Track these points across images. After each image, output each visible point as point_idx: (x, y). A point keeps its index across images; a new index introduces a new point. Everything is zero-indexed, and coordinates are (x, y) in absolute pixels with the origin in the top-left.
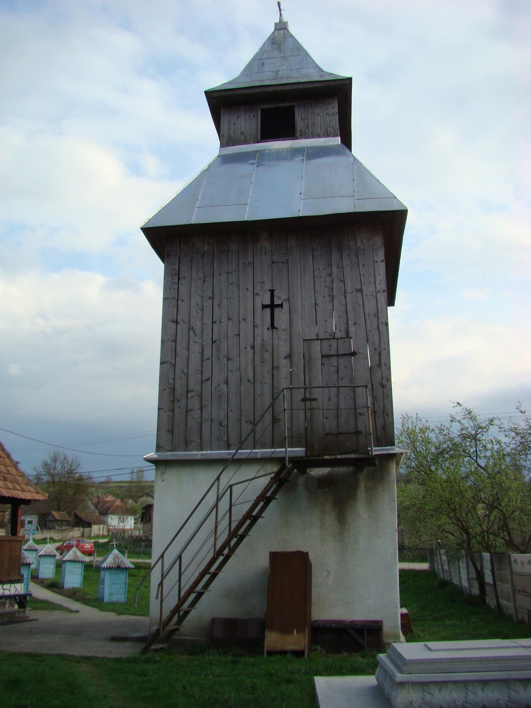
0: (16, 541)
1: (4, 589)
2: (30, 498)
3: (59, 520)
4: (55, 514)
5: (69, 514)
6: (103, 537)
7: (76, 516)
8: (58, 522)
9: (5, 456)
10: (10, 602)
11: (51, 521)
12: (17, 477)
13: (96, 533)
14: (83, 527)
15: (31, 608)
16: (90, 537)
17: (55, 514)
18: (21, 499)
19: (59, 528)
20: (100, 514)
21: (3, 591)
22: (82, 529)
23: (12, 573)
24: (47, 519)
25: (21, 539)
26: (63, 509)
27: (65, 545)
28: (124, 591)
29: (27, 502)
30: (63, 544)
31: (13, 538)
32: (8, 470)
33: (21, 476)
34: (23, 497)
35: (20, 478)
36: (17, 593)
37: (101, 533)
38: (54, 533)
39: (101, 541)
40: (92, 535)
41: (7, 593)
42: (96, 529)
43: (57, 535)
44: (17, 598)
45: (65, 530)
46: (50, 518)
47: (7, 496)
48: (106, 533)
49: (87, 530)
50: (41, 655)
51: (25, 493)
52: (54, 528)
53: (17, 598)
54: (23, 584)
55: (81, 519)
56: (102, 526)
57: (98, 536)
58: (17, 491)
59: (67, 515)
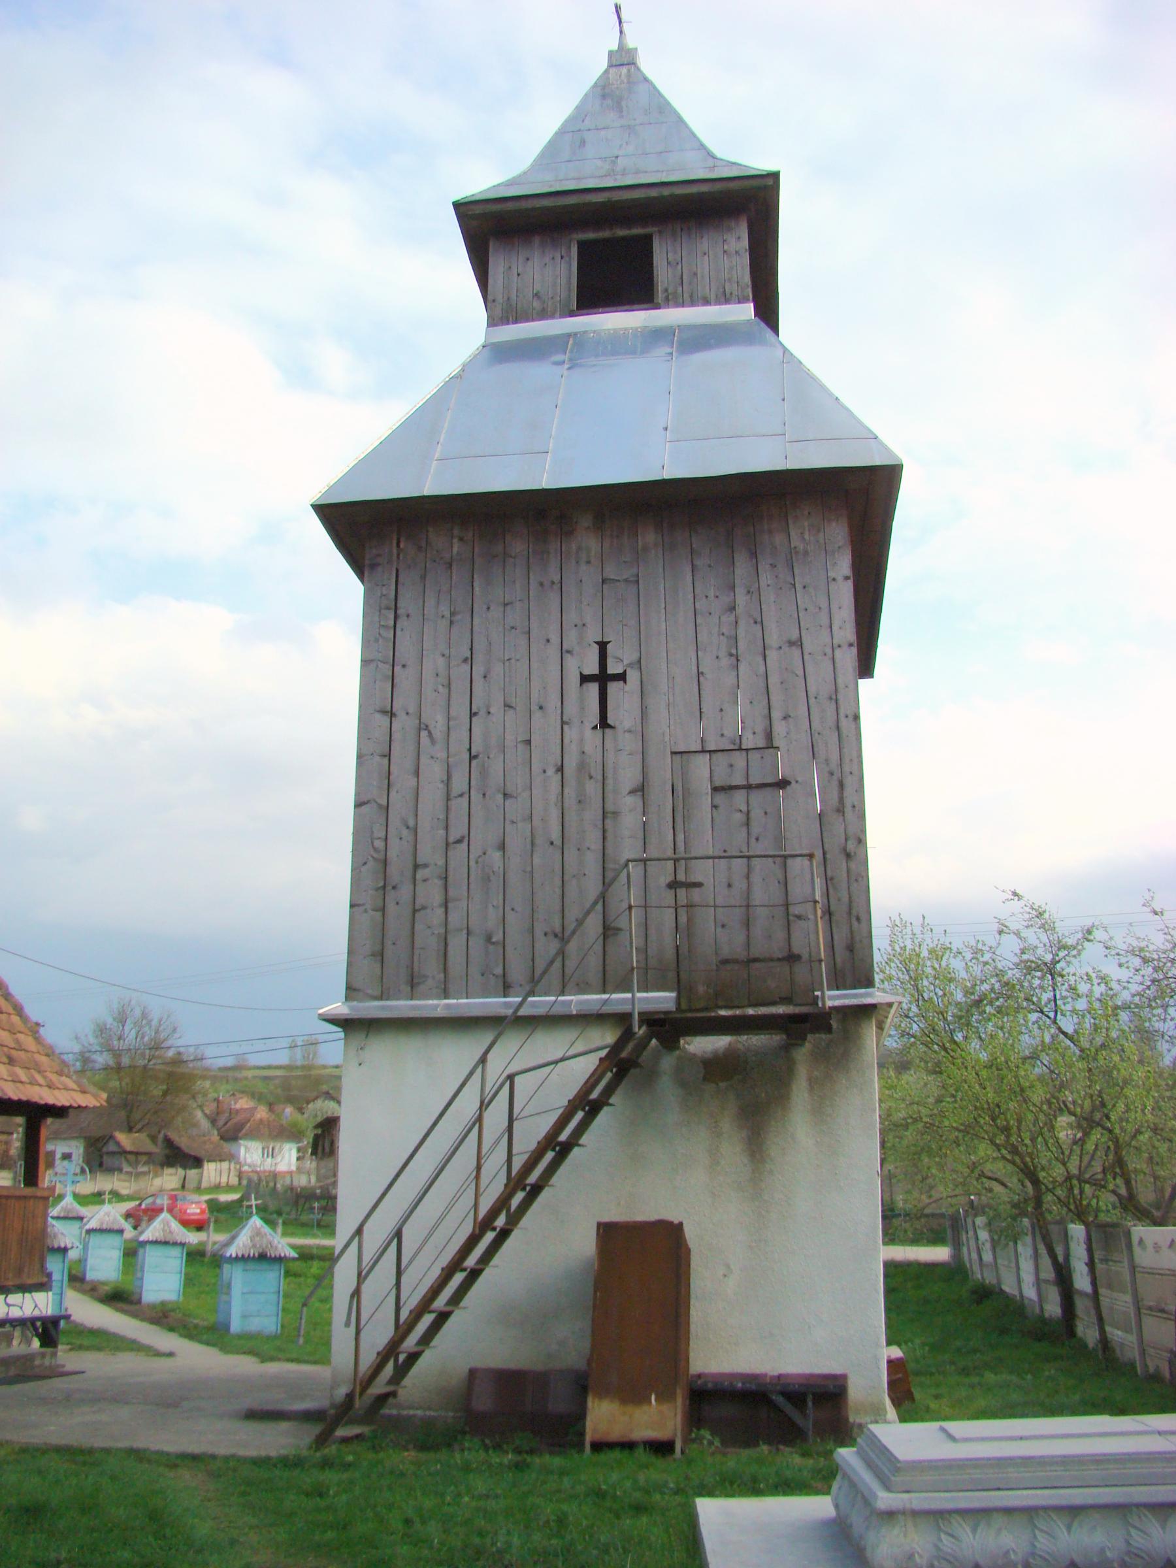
0: (36, 1197)
1: (9, 1305)
2: (67, 1104)
3: (130, 1153)
4: (123, 1138)
5: (153, 1138)
6: (229, 1188)
7: (169, 1142)
8: (129, 1156)
9: (11, 1010)
10: (23, 1334)
11: (113, 1153)
12: (36, 1056)
13: (213, 1179)
14: (185, 1167)
15: (69, 1347)
16: (198, 1189)
17: (123, 1138)
18: (46, 1105)
19: (130, 1169)
20: (222, 1138)
21: (6, 1309)
22: (181, 1171)
23: (26, 1270)
24: (105, 1149)
25: (46, 1194)
26: (139, 1126)
27: (143, 1206)
28: (275, 1308)
29: (59, 1112)
30: (140, 1205)
31: (29, 1191)
32: (17, 1041)
33: (47, 1055)
34: (51, 1101)
35: (43, 1059)
36: (37, 1313)
37: (224, 1180)
38: (119, 1180)
39: (224, 1198)
40: (204, 1184)
41: (16, 1313)
42: (212, 1172)
43: (127, 1184)
44: (39, 1324)
45: (144, 1173)
46: (112, 1147)
47: (15, 1098)
48: (234, 1180)
49: (192, 1173)
50: (91, 1451)
51: (56, 1092)
52: (120, 1170)
53: (39, 1324)
54: (50, 1293)
55: (178, 1148)
56: (225, 1165)
57: (217, 1188)
58: (37, 1088)
59: (148, 1141)
